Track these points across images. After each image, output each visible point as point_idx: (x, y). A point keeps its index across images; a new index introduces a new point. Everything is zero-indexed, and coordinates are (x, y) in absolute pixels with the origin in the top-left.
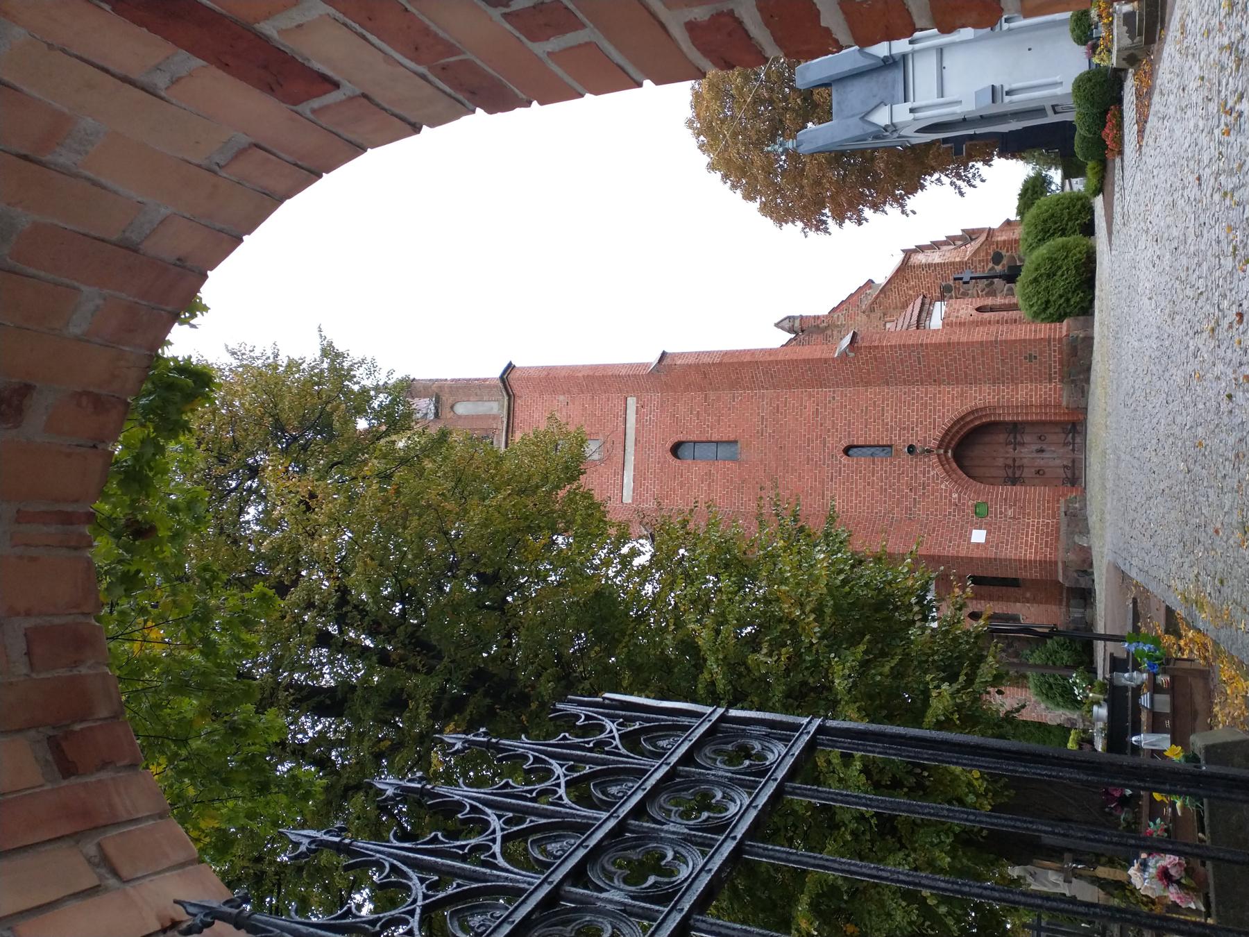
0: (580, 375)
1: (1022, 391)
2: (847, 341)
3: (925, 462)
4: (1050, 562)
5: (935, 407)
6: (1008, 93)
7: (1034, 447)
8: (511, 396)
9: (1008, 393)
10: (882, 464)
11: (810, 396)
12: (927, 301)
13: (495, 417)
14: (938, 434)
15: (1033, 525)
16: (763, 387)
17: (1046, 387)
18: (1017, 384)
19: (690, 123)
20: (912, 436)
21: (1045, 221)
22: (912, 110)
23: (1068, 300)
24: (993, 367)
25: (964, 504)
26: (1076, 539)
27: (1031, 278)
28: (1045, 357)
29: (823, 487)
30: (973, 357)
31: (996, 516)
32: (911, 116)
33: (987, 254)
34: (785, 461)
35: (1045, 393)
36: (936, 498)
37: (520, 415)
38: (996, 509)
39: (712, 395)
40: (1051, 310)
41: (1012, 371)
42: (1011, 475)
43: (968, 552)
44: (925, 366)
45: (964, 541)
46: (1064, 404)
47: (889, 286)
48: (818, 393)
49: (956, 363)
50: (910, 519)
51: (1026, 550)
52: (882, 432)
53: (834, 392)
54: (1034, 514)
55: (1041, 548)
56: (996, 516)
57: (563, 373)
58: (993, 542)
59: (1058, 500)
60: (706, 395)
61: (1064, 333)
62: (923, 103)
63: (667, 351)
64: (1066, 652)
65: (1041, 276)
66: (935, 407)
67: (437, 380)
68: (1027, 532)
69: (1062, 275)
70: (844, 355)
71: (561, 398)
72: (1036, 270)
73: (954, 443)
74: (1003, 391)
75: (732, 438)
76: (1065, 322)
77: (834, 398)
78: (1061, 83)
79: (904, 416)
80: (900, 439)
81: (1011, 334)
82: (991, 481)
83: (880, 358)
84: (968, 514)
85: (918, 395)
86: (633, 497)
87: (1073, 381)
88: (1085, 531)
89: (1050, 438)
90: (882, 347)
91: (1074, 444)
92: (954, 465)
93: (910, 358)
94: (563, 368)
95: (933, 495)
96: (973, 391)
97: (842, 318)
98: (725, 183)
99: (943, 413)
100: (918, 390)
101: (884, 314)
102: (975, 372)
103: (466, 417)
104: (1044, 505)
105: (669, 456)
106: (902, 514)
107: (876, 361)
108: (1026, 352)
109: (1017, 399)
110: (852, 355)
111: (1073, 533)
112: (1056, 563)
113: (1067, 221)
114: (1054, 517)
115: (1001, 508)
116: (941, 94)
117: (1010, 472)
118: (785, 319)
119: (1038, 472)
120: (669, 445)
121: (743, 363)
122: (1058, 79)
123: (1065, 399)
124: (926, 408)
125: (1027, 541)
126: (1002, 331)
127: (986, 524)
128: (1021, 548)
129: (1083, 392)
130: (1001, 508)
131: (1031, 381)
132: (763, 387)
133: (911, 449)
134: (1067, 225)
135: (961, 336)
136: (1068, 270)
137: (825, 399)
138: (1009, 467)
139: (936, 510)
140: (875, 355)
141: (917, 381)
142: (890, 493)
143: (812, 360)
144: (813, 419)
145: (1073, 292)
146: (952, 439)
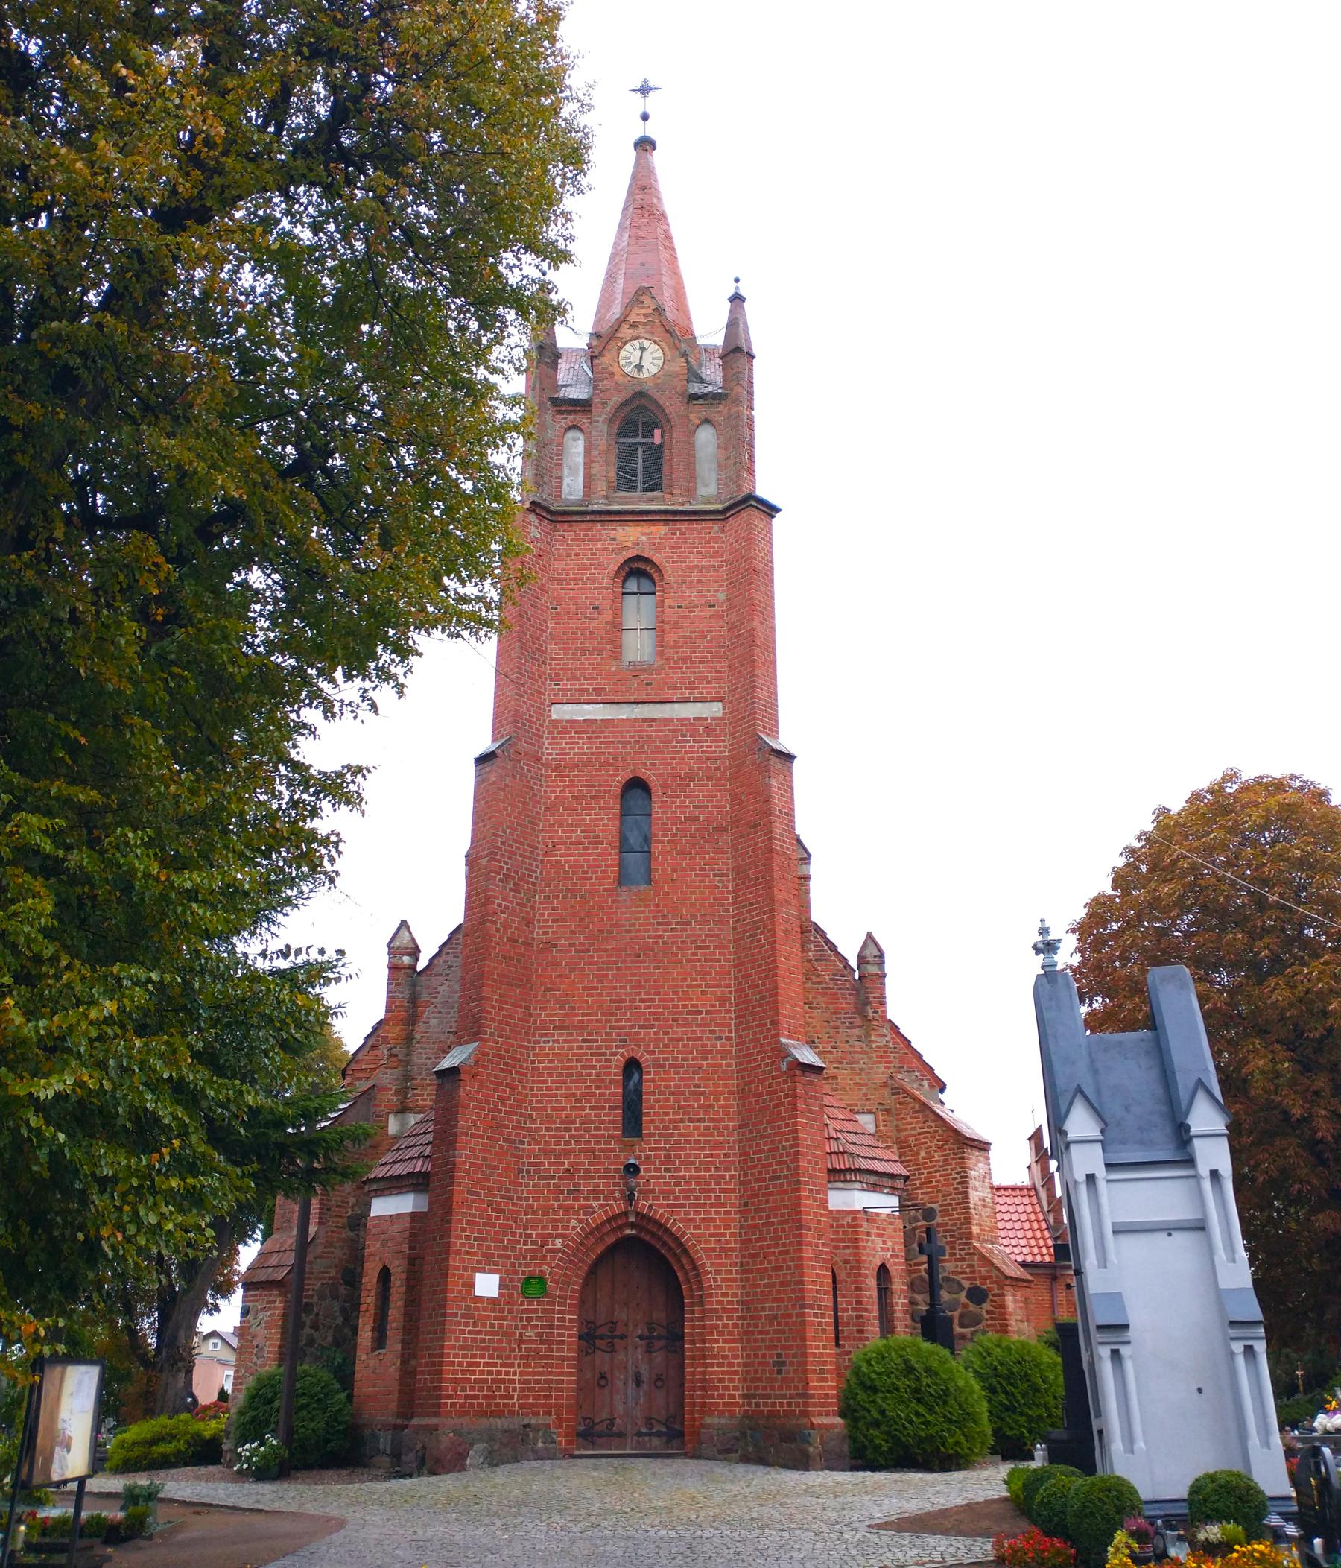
0: (756, 623)
2: (807, 1056)
3: (612, 1192)
4: (439, 1405)
6: (1115, 1353)
7: (644, 1370)
8: (722, 515)
9: (725, 1326)
10: (610, 1122)
11: (723, 999)
12: (899, 1183)
13: (690, 491)
14: (659, 1213)
15: (507, 1373)
16: (737, 921)
17: (735, 1388)
18: (741, 1340)
19: (1232, 776)
20: (656, 1170)
21: (1026, 1377)
22: (1091, 1178)
23: (876, 1424)
24: (766, 1301)
25: (544, 1258)
26: (480, 1446)
27: (913, 1361)
28: (780, 1388)
29: (575, 1028)
30: (780, 1268)
31: (524, 1311)
32: (1080, 1177)
33: (984, 1278)
34: (616, 962)
35: (726, 1388)
36: (555, 1213)
37: (694, 532)
38: (536, 1311)
39: (725, 840)
40: (862, 1396)
41: (761, 1332)
42: (599, 1332)
43: (457, 1268)
44: (767, 1187)
45: (479, 1262)
46: (708, 1420)
47: (932, 1116)
48: (728, 1012)
49: (772, 1239)
50: (521, 1171)
51: (460, 1364)
52: (662, 1121)
53: (729, 1039)
54: (528, 1374)
55: (463, 1389)
56: (524, 1311)
57: (759, 597)
58: (476, 1309)
59: (549, 1413)
60: (726, 829)
61: (817, 1421)
62: (1104, 1200)
63: (796, 764)
64: (322, 1425)
65: (918, 1379)
66: (704, 1205)
67: (751, 394)
68: (495, 1364)
69: (918, 1414)
70: (782, 1053)
71: (722, 596)
72: (928, 1370)
73: (647, 1238)
74: (730, 1318)
75: (656, 875)
76: (839, 1420)
77: (719, 1038)
78: (1132, 1452)
79: (688, 1156)
81: (816, 1331)
82: (585, 1301)
83: (779, 1112)
84: (528, 1265)
85: (723, 1177)
86: (561, 721)
87: (744, 1434)
88: (493, 1460)
89: (660, 1397)
90: (795, 1117)
91: (650, 1435)
92: (611, 1240)
93: (779, 1163)
94: (770, 596)
95: (560, 1206)
96: (730, 1268)
97: (882, 1041)
98: (1139, 838)
99: (693, 1220)
101: (888, 1111)
102: (759, 1271)
103: (691, 445)
104: (542, 1389)
105: (625, 775)
106: (528, 1157)
107: (776, 1106)
108: (787, 1355)
109: (717, 1341)
110: (784, 1066)
111: (491, 1439)
112: (437, 1414)
113: (1027, 1415)
114: (521, 1407)
115: (538, 1319)
116: (1118, 1231)
117: (604, 1331)
118: (879, 949)
119: (603, 1377)
120: (644, 773)
121: (771, 887)
122: (1140, 1445)
123: (716, 1421)
124: (702, 1191)
125: (478, 1364)
126: (823, 1316)
127: (511, 1295)
128: (465, 1356)
129: (728, 1451)
130: (538, 1319)
131: (745, 1365)
132: (737, 921)
133: (632, 1170)
134: (1021, 1414)
135: (815, 1248)
136: (926, 1423)
137: (717, 1025)
138: (612, 1330)
139: (535, 1213)
140: (782, 1105)
141: (746, 1175)
142: (563, 1137)
143: (776, 1002)
144: (685, 1006)
145: (888, 1433)
146: (653, 1235)
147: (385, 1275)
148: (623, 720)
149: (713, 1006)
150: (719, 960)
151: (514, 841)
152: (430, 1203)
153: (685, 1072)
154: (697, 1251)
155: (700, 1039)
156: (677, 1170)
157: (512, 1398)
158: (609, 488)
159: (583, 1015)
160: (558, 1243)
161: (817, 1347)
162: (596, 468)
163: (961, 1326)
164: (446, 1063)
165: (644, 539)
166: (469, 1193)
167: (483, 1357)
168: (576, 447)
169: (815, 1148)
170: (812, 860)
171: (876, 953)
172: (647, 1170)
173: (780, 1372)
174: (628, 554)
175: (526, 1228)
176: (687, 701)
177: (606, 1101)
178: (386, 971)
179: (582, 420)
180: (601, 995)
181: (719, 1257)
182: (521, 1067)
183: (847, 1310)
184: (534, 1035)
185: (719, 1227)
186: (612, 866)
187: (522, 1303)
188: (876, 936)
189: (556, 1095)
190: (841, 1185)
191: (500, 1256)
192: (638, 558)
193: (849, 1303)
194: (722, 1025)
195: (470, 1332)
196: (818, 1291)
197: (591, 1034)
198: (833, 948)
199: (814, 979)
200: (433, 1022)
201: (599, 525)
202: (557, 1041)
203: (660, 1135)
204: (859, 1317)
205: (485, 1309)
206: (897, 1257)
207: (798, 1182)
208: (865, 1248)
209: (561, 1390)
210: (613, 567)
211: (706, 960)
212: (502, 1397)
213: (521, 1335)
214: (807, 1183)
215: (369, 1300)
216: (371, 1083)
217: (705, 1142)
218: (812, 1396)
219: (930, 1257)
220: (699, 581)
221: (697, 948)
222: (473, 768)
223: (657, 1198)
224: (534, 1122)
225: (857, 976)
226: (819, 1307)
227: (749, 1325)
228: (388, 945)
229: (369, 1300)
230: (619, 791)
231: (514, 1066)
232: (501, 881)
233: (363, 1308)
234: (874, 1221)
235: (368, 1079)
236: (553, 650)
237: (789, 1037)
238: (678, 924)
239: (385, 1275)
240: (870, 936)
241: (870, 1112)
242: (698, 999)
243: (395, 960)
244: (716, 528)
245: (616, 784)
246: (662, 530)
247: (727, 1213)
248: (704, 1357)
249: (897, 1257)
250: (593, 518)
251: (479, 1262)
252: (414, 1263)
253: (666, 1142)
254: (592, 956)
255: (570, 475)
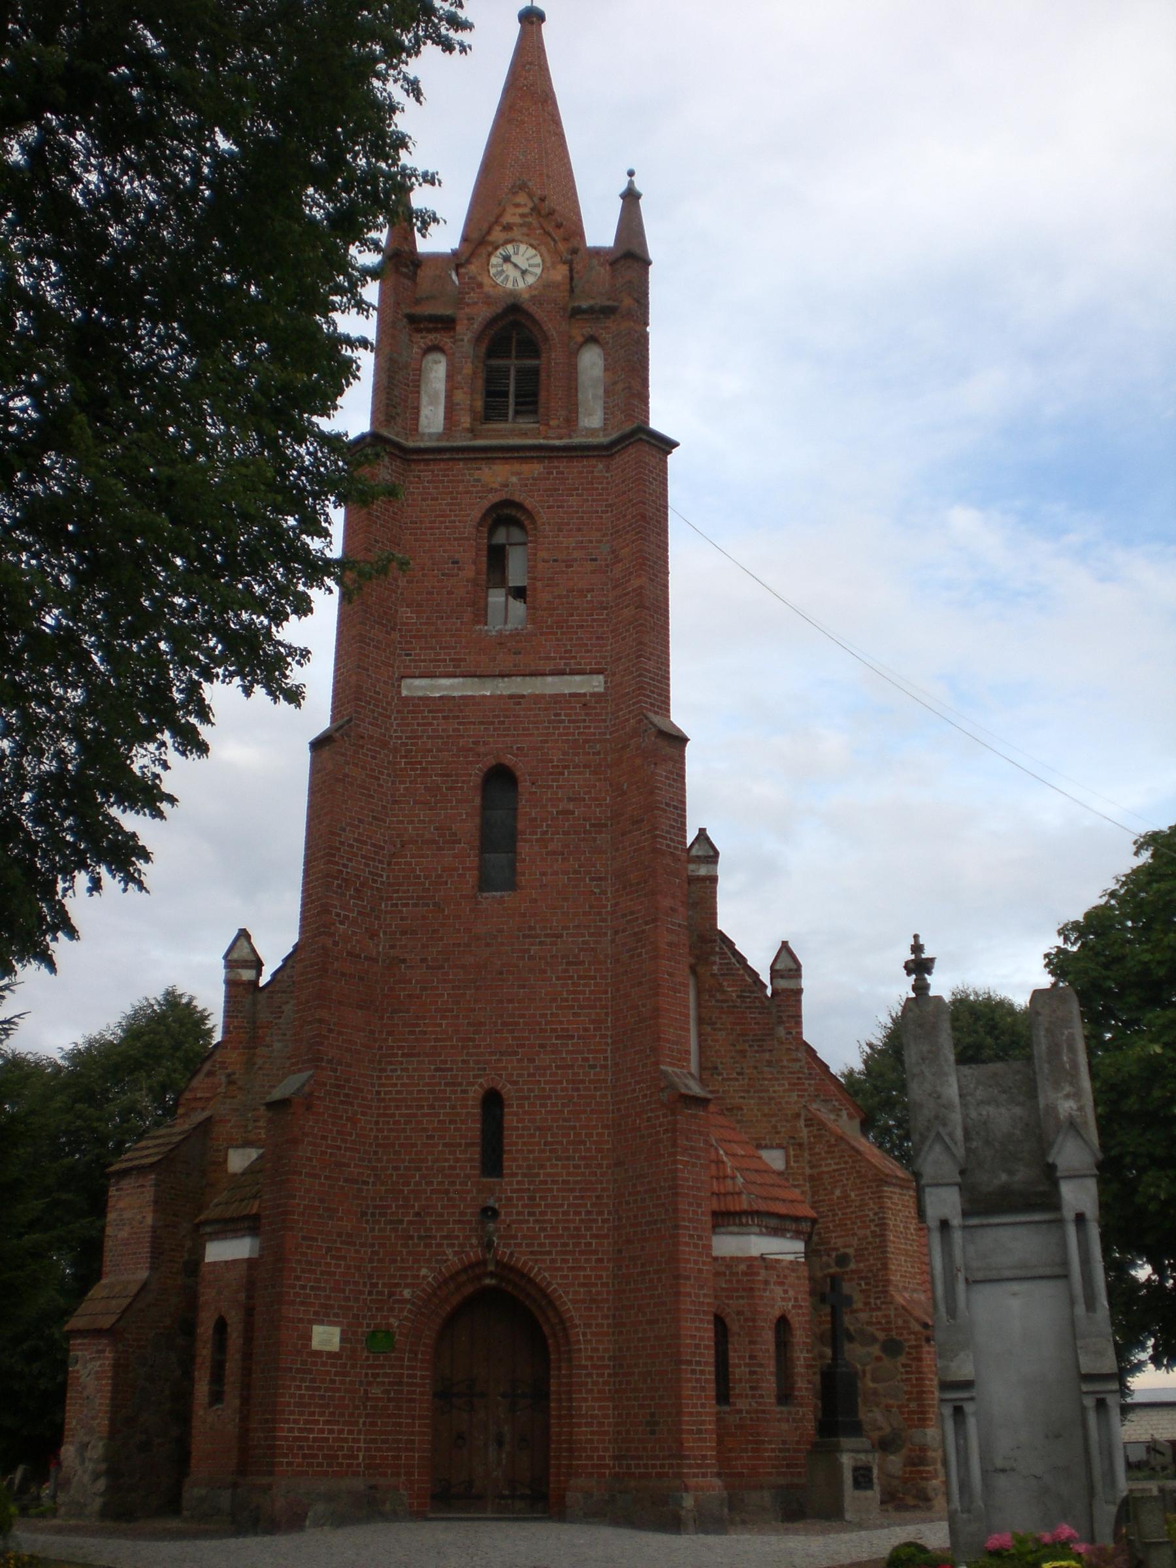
1: (600, 1408)
5: (572, 1253)
9: (595, 1383)
12: (805, 1227)
13: (571, 421)
17: (606, 1449)
31: (369, 1367)
35: (596, 1449)
38: (382, 1366)
45: (316, 1313)
48: (604, 1036)
51: (296, 1421)
52: (525, 1159)
53: (604, 1067)
56: (369, 1367)
60: (605, 825)
68: (337, 1423)
77: (593, 1067)
80: (513, 1191)
85: (596, 1221)
86: (413, 698)
90: (674, 1154)
92: (469, 1290)
95: (409, 1253)
97: (796, 1066)
100: (604, 1221)
112: (271, 1473)
114: (368, 1467)
115: (386, 1375)
120: (509, 760)
126: (702, 1372)
128: (301, 1413)
130: (386, 1375)
137: (589, 1051)
141: (620, 1219)
144: (554, 1030)
147: (221, 1326)
148: (484, 696)
149: (585, 1030)
150: (595, 978)
151: (356, 840)
152: (262, 1249)
153: (553, 1105)
154: (564, 1303)
155: (572, 1067)
156: (542, 1213)
157: (357, 1457)
158: (474, 419)
159: (436, 1040)
160: (407, 1293)
161: (695, 1406)
162: (460, 396)
163: (874, 1380)
164: (277, 1094)
165: (514, 479)
166: (304, 1238)
167: (322, 1414)
168: (437, 372)
169: (698, 1189)
170: (720, 859)
171: (794, 967)
172: (508, 1214)
173: (653, 1432)
174: (494, 498)
175: (370, 1277)
176: (562, 673)
177: (462, 1137)
178: (223, 987)
179: (445, 339)
180: (457, 1017)
181: (590, 1309)
182: (364, 1098)
183: (739, 1366)
184: (380, 1062)
185: (589, 1277)
186: (470, 869)
187: (367, 1358)
188: (791, 945)
189: (404, 1130)
190: (735, 1229)
191: (340, 1307)
192: (508, 503)
193: (742, 1358)
194: (595, 1051)
195: (307, 1388)
196: (697, 1346)
197: (445, 1062)
198: (742, 960)
199: (719, 996)
200: (277, 1045)
201: (461, 465)
202: (406, 1070)
203: (524, 1175)
204: (752, 1373)
205: (324, 1364)
206: (801, 1307)
207: (677, 1227)
208: (761, 1298)
209: (413, 1450)
210: (477, 514)
211: (579, 977)
212: (344, 1457)
213: (366, 1391)
214: (687, 1228)
215: (205, 1352)
216: (206, 1114)
217: (576, 1182)
218: (688, 1457)
219: (833, 1307)
220: (579, 530)
221: (568, 963)
222: (308, 754)
223: (520, 1245)
224: (379, 1160)
225: (769, 992)
226: (698, 1363)
227: (620, 1383)
228: (226, 957)
229: (205, 1352)
230: (479, 780)
231: (357, 1098)
232: (340, 886)
233: (199, 1360)
234: (774, 1268)
235: (203, 1109)
236: (406, 614)
237: (671, 1064)
238: (546, 936)
239: (221, 1326)
240: (785, 944)
241: (779, 1146)
242: (569, 1022)
243: (232, 976)
244: (600, 466)
245: (476, 773)
246: (537, 469)
247: (600, 1260)
248: (572, 1416)
249: (801, 1307)
250: (579, 454)
251: (316, 1313)
252: (249, 1312)
253: (530, 1183)
254: (447, 974)
255: (431, 404)
